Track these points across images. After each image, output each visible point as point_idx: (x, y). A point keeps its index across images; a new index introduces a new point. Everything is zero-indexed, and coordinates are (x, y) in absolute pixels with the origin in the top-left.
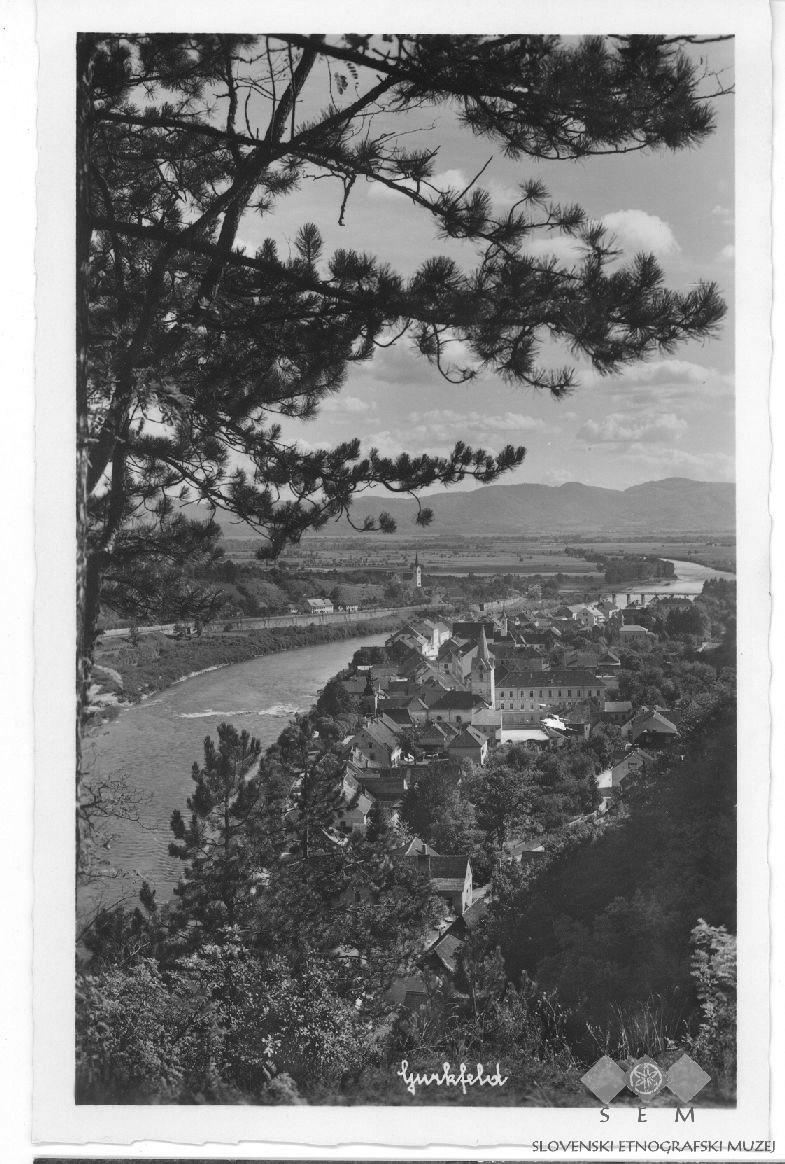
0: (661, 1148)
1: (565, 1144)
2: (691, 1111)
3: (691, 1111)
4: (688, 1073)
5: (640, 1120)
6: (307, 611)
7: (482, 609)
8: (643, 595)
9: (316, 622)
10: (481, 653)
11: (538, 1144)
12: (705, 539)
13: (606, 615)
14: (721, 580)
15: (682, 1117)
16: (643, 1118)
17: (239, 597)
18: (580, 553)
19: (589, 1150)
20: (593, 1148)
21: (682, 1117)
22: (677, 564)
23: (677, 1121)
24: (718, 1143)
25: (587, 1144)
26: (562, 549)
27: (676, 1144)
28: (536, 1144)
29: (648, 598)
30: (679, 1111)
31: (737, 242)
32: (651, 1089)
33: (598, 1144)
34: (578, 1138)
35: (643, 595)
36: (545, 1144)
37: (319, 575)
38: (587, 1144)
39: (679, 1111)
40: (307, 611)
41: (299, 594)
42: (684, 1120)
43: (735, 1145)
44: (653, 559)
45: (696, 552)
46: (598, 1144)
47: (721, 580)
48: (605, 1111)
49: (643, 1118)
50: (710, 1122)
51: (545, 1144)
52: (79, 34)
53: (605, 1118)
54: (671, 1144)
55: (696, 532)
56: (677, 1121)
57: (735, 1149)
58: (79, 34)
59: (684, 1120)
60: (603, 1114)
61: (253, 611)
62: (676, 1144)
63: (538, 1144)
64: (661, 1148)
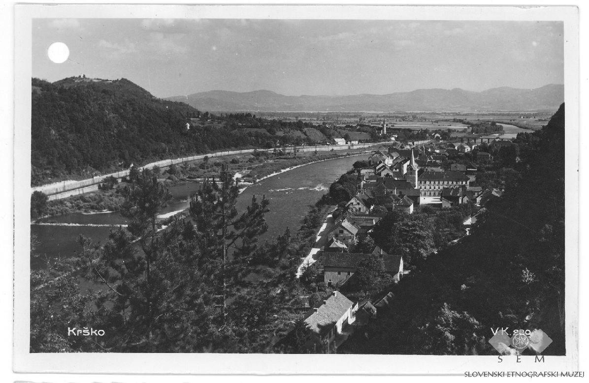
0: (528, 375)
1: (481, 373)
2: (543, 357)
3: (543, 357)
4: (537, 338)
5: (517, 362)
6: (334, 143)
7: (414, 144)
8: (489, 139)
9: (335, 148)
10: (411, 163)
11: (467, 373)
12: (518, 114)
13: (471, 148)
14: (526, 133)
15: (538, 360)
16: (519, 360)
17: (303, 136)
18: (461, 121)
19: (493, 376)
20: (495, 375)
21: (538, 360)
22: (503, 125)
23: (536, 362)
24: (556, 373)
25: (491, 373)
26: (453, 118)
27: (535, 373)
28: (466, 373)
29: (491, 141)
30: (537, 357)
31: (30, 226)
32: (523, 346)
33: (497, 373)
34: (487, 370)
35: (489, 139)
36: (471, 373)
37: (341, 128)
38: (491, 373)
39: (537, 357)
40: (334, 143)
41: (330, 135)
42: (539, 361)
43: (564, 373)
44: (494, 123)
45: (514, 120)
46: (497, 373)
47: (526, 133)
48: (500, 357)
49: (519, 360)
50: (552, 362)
51: (471, 373)
52: (31, 352)
53: (500, 361)
54: (533, 373)
55: (514, 112)
56: (536, 362)
57: (564, 376)
58: (31, 352)
59: (539, 361)
60: (499, 358)
61: (311, 143)
62: (535, 373)
63: (467, 373)
64: (528, 375)
